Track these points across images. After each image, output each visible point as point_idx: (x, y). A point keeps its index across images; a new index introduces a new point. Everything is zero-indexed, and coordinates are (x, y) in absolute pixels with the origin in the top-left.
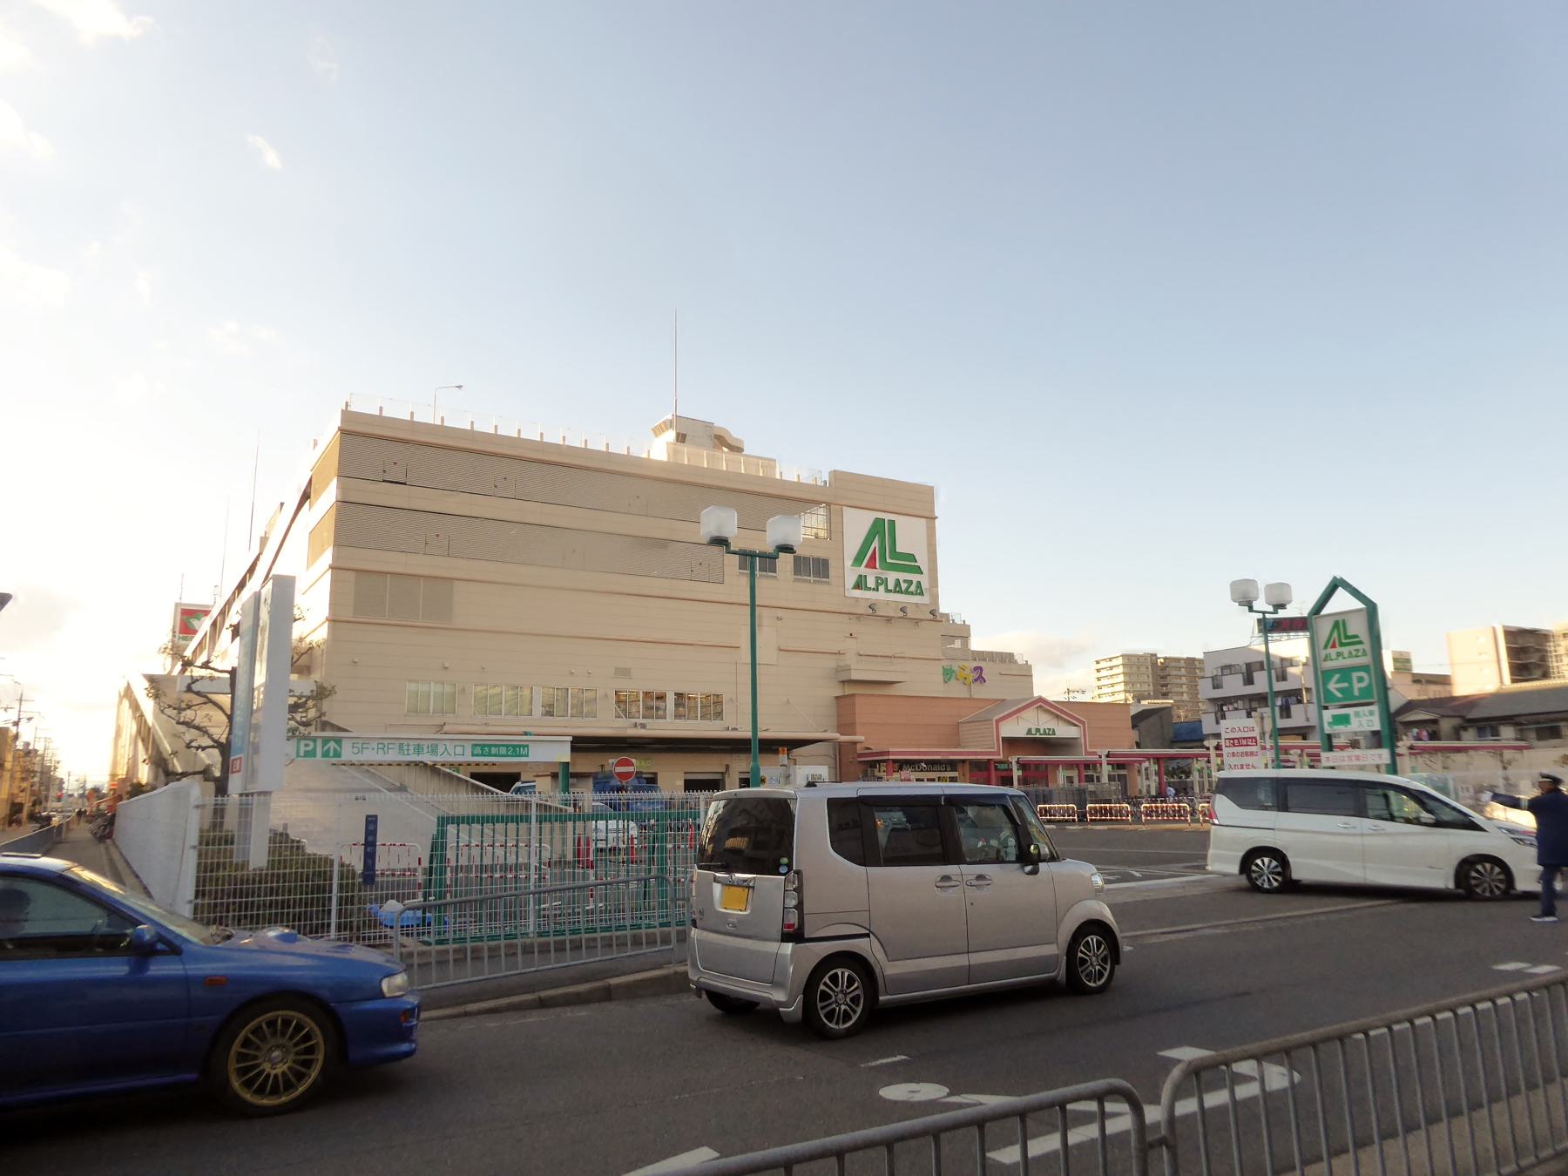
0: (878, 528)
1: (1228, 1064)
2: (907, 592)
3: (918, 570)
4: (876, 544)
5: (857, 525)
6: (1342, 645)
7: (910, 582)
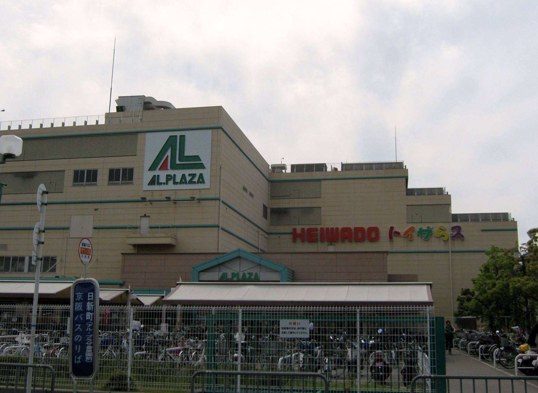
0: (171, 143)
1: (92, 345)
2: (191, 182)
3: (202, 166)
4: (169, 153)
5: (153, 145)
6: (174, 167)
7: (193, 176)
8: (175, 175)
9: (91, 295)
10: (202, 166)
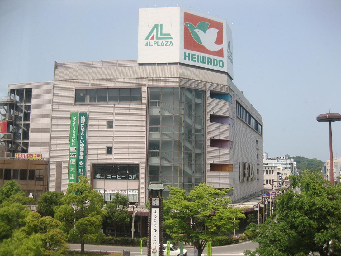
4: (155, 31)
6: (157, 38)
8: (158, 42)
9: (131, 176)
10: (171, 38)
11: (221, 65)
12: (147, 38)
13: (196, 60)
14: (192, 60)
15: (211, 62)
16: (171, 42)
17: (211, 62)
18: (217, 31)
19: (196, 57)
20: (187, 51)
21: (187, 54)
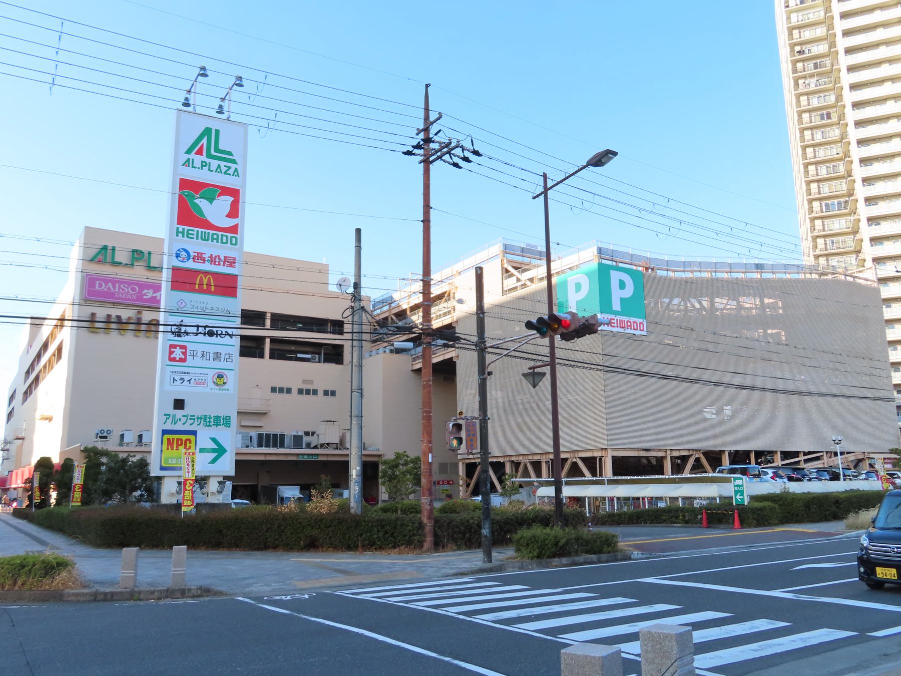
4: (205, 139)
10: (234, 162)
11: (234, 242)
12: (189, 152)
13: (195, 237)
14: (188, 237)
15: (217, 240)
16: (236, 170)
17: (217, 240)
18: (232, 199)
19: (195, 233)
20: (181, 227)
21: (181, 230)
